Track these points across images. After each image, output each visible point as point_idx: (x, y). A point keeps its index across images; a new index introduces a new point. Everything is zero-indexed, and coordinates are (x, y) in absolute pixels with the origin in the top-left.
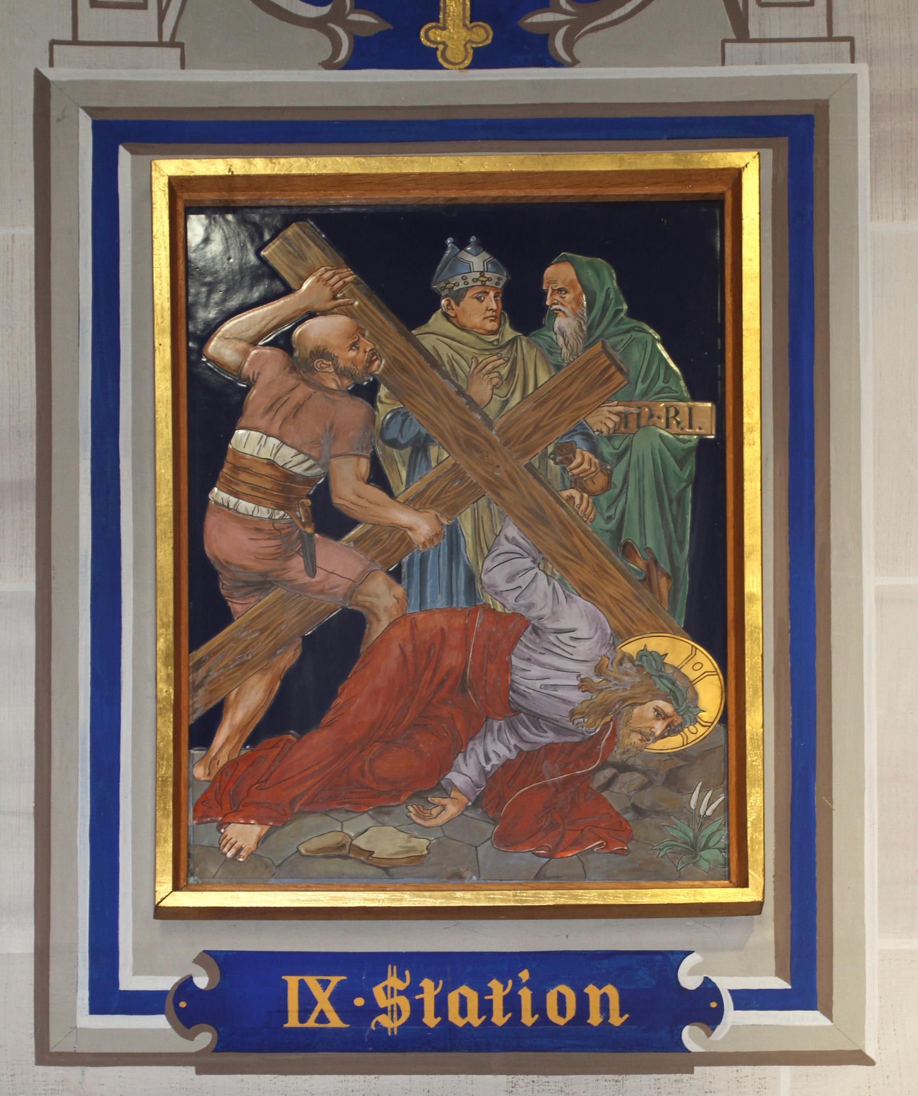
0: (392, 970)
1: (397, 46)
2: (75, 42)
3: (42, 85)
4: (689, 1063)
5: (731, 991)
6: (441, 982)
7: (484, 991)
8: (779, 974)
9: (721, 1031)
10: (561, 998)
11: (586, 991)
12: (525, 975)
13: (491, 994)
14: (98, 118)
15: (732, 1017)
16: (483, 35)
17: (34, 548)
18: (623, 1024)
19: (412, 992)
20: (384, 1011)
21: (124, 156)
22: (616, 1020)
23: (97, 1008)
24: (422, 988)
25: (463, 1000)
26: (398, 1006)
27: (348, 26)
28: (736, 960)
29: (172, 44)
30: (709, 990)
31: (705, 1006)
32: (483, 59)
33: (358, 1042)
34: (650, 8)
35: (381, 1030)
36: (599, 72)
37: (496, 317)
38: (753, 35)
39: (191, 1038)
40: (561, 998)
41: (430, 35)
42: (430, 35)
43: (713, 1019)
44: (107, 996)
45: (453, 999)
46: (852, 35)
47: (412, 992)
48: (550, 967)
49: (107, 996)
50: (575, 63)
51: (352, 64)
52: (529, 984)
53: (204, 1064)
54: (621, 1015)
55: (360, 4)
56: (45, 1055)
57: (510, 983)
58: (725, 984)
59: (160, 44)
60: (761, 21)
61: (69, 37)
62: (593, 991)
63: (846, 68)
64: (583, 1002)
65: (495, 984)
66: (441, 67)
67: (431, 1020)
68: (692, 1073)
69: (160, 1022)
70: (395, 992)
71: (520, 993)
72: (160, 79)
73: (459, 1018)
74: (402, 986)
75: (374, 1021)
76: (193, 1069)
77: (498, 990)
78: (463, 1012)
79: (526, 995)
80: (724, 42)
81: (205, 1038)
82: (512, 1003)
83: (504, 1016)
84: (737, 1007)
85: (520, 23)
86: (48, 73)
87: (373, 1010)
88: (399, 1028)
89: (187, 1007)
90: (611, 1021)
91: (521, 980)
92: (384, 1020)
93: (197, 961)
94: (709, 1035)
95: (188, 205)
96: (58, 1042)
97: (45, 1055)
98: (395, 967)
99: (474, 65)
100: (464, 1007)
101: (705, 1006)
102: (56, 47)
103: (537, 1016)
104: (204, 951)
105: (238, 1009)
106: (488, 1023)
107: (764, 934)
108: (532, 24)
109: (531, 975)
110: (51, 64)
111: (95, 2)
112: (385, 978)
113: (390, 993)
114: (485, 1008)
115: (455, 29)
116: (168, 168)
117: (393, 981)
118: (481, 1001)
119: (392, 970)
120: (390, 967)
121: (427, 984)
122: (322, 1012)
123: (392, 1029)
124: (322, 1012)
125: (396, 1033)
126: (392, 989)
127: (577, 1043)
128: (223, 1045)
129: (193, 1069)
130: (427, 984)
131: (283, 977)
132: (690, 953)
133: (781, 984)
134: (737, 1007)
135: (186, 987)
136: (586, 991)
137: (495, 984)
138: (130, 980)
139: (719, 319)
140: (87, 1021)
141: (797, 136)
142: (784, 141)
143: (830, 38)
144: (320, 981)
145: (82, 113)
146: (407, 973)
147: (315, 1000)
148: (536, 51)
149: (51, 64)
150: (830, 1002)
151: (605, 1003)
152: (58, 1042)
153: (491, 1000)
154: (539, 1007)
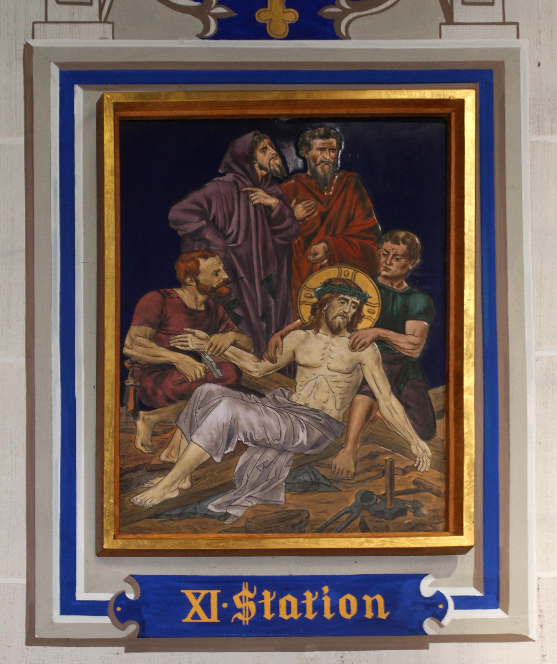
0: (245, 586)
1: (242, 23)
2: (46, 22)
3: (28, 50)
5: (454, 598)
6: (275, 593)
7: (301, 598)
8: (476, 586)
9: (446, 621)
10: (348, 602)
12: (326, 589)
14: (64, 70)
15: (453, 614)
16: (292, 16)
19: (259, 597)
20: (240, 610)
21: (79, 91)
22: (382, 615)
23: (64, 612)
25: (289, 604)
28: (452, 581)
29: (106, 22)
31: (436, 607)
32: (296, 32)
33: (225, 631)
36: (361, 42)
39: (123, 629)
40: (348, 602)
41: (261, 16)
42: (261, 16)
43: (440, 616)
44: (70, 605)
45: (282, 602)
48: (341, 585)
49: (70, 605)
51: (216, 37)
52: (328, 594)
53: (131, 645)
54: (385, 612)
56: (32, 640)
58: (448, 592)
59: (101, 22)
60: (461, 12)
61: (43, 19)
62: (368, 599)
64: (361, 605)
65: (308, 594)
67: (268, 615)
68: (427, 648)
69: (105, 620)
71: (324, 599)
72: (91, 40)
73: (286, 615)
74: (252, 596)
75: (234, 617)
76: (123, 649)
78: (289, 611)
79: (327, 600)
81: (133, 628)
82: (318, 607)
85: (319, 13)
87: (234, 609)
89: (123, 610)
91: (322, 592)
92: (239, 616)
93: (126, 580)
97: (32, 640)
99: (290, 37)
100: (289, 607)
101: (436, 607)
102: (36, 26)
104: (131, 576)
105: (153, 613)
107: (467, 565)
110: (33, 37)
113: (244, 603)
114: (302, 609)
115: (278, 13)
117: (246, 592)
119: (245, 586)
120: (244, 583)
121: (266, 594)
123: (246, 621)
125: (247, 623)
126: (245, 597)
129: (123, 649)
130: (266, 594)
131: (182, 591)
132: (427, 575)
135: (121, 597)
137: (308, 594)
138: (82, 594)
140: (59, 618)
141: (486, 78)
143: (504, 23)
144: (194, 594)
145: (53, 65)
146: (255, 588)
147: (198, 608)
148: (327, 30)
149: (33, 37)
151: (377, 606)
154: (335, 608)
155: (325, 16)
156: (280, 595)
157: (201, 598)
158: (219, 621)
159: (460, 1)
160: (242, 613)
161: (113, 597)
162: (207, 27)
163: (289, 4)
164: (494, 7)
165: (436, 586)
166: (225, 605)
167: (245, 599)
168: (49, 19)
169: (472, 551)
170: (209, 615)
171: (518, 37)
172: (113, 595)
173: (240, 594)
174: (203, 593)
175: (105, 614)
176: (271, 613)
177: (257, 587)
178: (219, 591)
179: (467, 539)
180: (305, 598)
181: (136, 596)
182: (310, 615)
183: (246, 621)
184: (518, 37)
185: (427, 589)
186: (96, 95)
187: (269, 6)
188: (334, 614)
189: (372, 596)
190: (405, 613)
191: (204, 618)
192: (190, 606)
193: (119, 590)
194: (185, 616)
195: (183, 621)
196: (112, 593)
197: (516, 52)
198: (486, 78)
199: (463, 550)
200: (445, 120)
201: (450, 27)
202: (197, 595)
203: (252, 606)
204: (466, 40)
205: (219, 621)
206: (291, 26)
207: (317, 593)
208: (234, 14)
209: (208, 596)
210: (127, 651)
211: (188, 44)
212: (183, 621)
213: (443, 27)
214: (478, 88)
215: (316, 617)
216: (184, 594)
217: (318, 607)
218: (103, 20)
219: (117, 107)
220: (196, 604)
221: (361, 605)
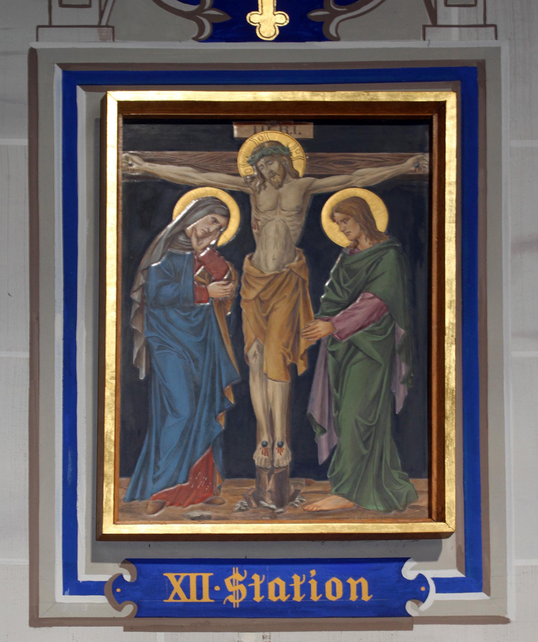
2: (50, 26)
3: (33, 54)
5: (434, 579)
6: (264, 576)
7: (289, 582)
8: (460, 570)
10: (334, 585)
11: (348, 581)
12: (313, 573)
13: (293, 583)
15: (433, 596)
16: (282, 19)
17: (395, 126)
18: (303, 599)
19: (247, 582)
20: (231, 593)
22: (366, 597)
24: (293, 579)
25: (277, 587)
26: (239, 591)
27: (208, 17)
29: (107, 26)
30: (421, 579)
31: (417, 590)
33: (217, 612)
34: (383, 4)
38: (440, 22)
39: (119, 609)
40: (334, 585)
41: (253, 18)
42: (253, 18)
43: (422, 598)
44: (73, 585)
45: (271, 586)
47: (247, 582)
49: (73, 585)
50: (338, 39)
51: (211, 39)
52: (315, 578)
55: (214, 6)
56: (36, 621)
58: (430, 574)
59: (99, 26)
60: (451, 15)
61: (47, 24)
63: (492, 43)
64: (347, 588)
65: (296, 578)
67: (258, 598)
69: (101, 599)
70: (237, 583)
71: (310, 582)
72: (88, 45)
74: (241, 578)
76: (122, 628)
77: (297, 581)
78: (277, 594)
79: (314, 584)
80: (424, 27)
81: (129, 609)
82: (305, 589)
84: (438, 591)
86: (35, 45)
87: (225, 592)
88: (240, 603)
89: (118, 590)
91: (310, 574)
94: (419, 607)
97: (36, 621)
100: (277, 590)
101: (417, 590)
103: (371, 596)
107: (450, 548)
109: (316, 572)
111: (61, 5)
114: (290, 591)
115: (268, 19)
116: (115, 97)
117: (237, 576)
120: (234, 568)
121: (256, 577)
123: (236, 603)
125: (238, 606)
126: (236, 580)
127: (344, 612)
128: (140, 613)
129: (122, 628)
130: (256, 577)
131: (165, 574)
133: (455, 573)
134: (438, 591)
135: (119, 580)
136: (348, 581)
137: (296, 578)
141: (469, 79)
143: (485, 25)
148: (318, 33)
150: (489, 588)
151: (184, 586)
154: (321, 590)
155: (309, 17)
158: (213, 601)
161: (111, 579)
162: (202, 29)
163: (279, 7)
165: (420, 569)
166: (217, 588)
167: (236, 582)
168: (54, 23)
169: (453, 537)
170: (188, 597)
171: (496, 38)
172: (110, 576)
174: (183, 575)
175: (102, 594)
177: (247, 571)
178: (212, 574)
179: (450, 523)
180: (292, 581)
181: (132, 579)
182: (315, 597)
183: (236, 603)
184: (496, 38)
185: (410, 571)
187: (260, 9)
191: (184, 599)
192: (171, 588)
196: (110, 574)
197: (497, 50)
198: (469, 79)
199: (447, 535)
202: (177, 578)
203: (243, 589)
205: (213, 601)
207: (304, 576)
208: (227, 18)
209: (187, 579)
210: (125, 630)
211: (187, 46)
213: (428, 30)
214: (459, 88)
216: (166, 577)
217: (305, 589)
221: (347, 588)
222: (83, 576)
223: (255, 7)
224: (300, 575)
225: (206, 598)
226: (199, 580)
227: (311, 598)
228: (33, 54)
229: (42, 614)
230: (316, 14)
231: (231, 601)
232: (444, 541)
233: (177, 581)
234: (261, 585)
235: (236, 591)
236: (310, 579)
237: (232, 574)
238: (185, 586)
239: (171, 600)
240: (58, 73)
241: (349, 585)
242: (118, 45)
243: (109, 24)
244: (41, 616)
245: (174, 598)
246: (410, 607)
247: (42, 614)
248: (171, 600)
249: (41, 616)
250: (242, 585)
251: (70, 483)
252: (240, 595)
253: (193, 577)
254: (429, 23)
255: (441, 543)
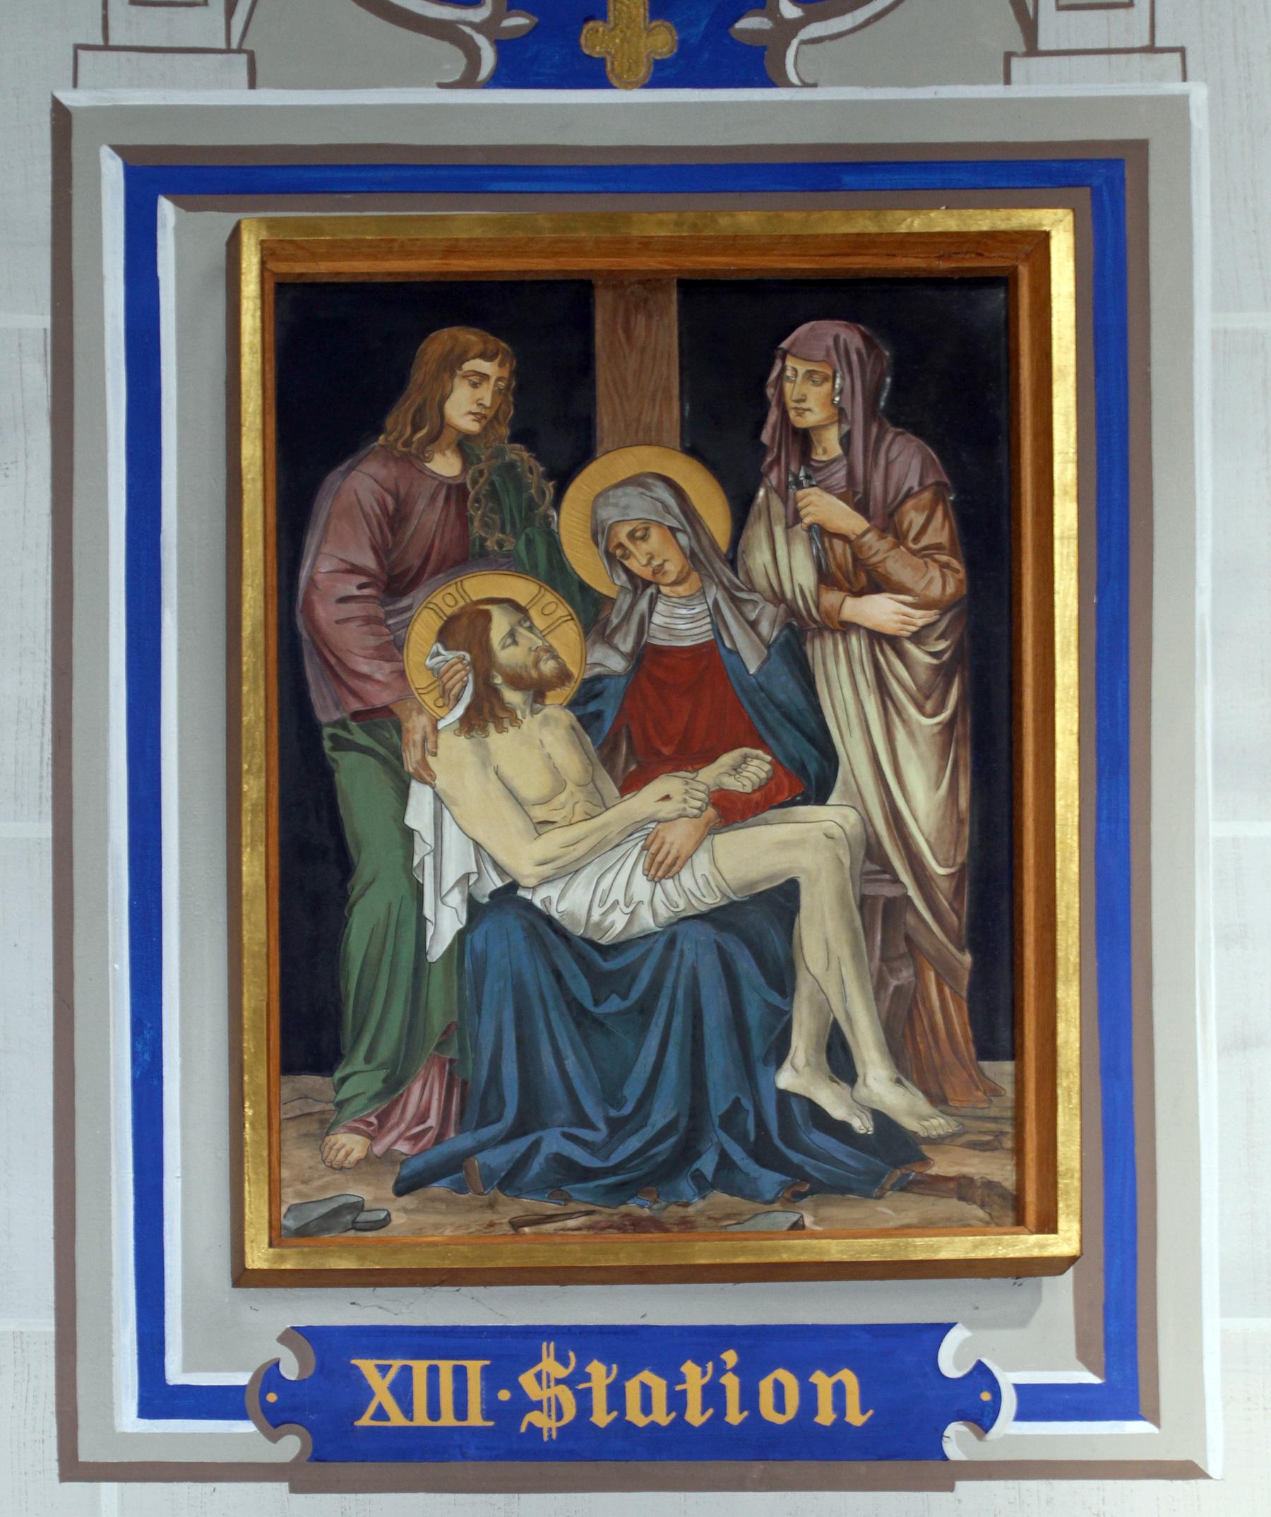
0: (548, 1348)
2: (106, 47)
3: (62, 118)
4: (946, 1475)
6: (615, 1367)
7: (675, 1378)
8: (1084, 1357)
10: (779, 1388)
11: (812, 1379)
12: (730, 1357)
13: (684, 1382)
16: (662, 41)
19: (575, 1381)
20: (538, 1406)
21: (167, 209)
22: (856, 1417)
23: (148, 1409)
25: (646, 1390)
28: (1034, 1343)
29: (240, 51)
31: (975, 1399)
32: (665, 75)
33: (505, 1449)
34: (902, 6)
35: (534, 1431)
36: (820, 97)
37: (484, 417)
38: (1043, 45)
40: (779, 1388)
43: (983, 1419)
44: (159, 1399)
45: (632, 1389)
46: (1184, 44)
47: (575, 1381)
48: (762, 1347)
49: (159, 1399)
51: (499, 80)
52: (735, 1370)
53: (299, 1478)
56: (73, 1468)
57: (710, 1366)
59: (229, 50)
60: (1055, 27)
62: (820, 1379)
63: (1175, 87)
64: (809, 1394)
66: (611, 86)
67: (601, 1417)
69: (246, 1427)
70: (552, 1383)
72: (207, 97)
74: (562, 1372)
76: (285, 1486)
78: (646, 1408)
79: (731, 1383)
80: (1008, 56)
82: (714, 1394)
83: (703, 1413)
86: (69, 98)
87: (524, 1404)
88: (559, 1429)
89: (274, 1402)
90: (848, 1419)
91: (725, 1363)
92: (535, 1418)
93: (284, 1339)
95: (281, 280)
96: (88, 1452)
97: (73, 1468)
98: (552, 1345)
99: (656, 82)
100: (647, 1399)
101: (975, 1399)
102: (81, 53)
103: (871, 1412)
104: (293, 1328)
105: (322, 1417)
106: (680, 1421)
108: (744, 31)
112: (538, 1359)
113: (544, 1381)
114: (677, 1401)
115: (630, 28)
117: (549, 1365)
118: (670, 1388)
119: (548, 1348)
120: (545, 1344)
121: (596, 1369)
122: (380, 1407)
123: (550, 1429)
124: (380, 1407)
125: (554, 1436)
126: (548, 1375)
127: (801, 1450)
129: (285, 1486)
130: (596, 1369)
131: (353, 1362)
135: (270, 1376)
136: (812, 1379)
139: (687, 407)
141: (1107, 182)
142: (1083, 195)
143: (1151, 49)
144: (378, 1366)
146: (572, 1354)
148: (755, 66)
152: (88, 1452)
153: (685, 1391)
154: (749, 1399)
156: (626, 1374)
157: (392, 1374)
158: (491, 1424)
159: (1053, 3)
160: (541, 1410)
164: (1133, 11)
166: (504, 1395)
167: (549, 1381)
168: (112, 42)
170: (408, 1411)
173: (537, 1369)
174: (397, 1364)
175: (242, 1415)
176: (741, 1411)
178: (487, 1362)
180: (682, 1380)
182: (695, 1416)
183: (550, 1429)
186: (217, 223)
188: (746, 1413)
189: (830, 1374)
190: (912, 1411)
191: (397, 1418)
192: (370, 1394)
193: (264, 1358)
194: (359, 1415)
195: (358, 1423)
197: (1180, 105)
199: (1055, 1266)
200: (1005, 281)
201: (1034, 61)
202: (384, 1370)
204: (1063, 90)
205: (491, 1424)
206: (659, 65)
209: (407, 1371)
212: (358, 1423)
213: (1016, 63)
215: (615, 1420)
216: (357, 1368)
217: (714, 1394)
218: (234, 45)
219: (268, 253)
220: (380, 1386)
222: (176, 1373)
223: (597, 11)
224: (701, 1362)
225: (475, 1418)
226: (460, 1375)
227: (593, 1419)
228: (62, 118)
229: (84, 1455)
230: (750, 23)
231: (538, 1425)
232: (1047, 1280)
233: (384, 1377)
234: (609, 1387)
235: (549, 1399)
236: (724, 1372)
237: (539, 1359)
238: (402, 1390)
239: (365, 1421)
240: (112, 171)
241: (814, 1387)
242: (266, 97)
243: (245, 47)
244: (83, 1457)
245: (374, 1418)
246: (957, 1440)
247: (84, 1455)
248: (365, 1421)
249: (83, 1457)
250: (564, 1387)
251: (929, 1172)
252: (560, 1416)
253: (420, 1368)
254: (1019, 45)
255: (1039, 1287)
